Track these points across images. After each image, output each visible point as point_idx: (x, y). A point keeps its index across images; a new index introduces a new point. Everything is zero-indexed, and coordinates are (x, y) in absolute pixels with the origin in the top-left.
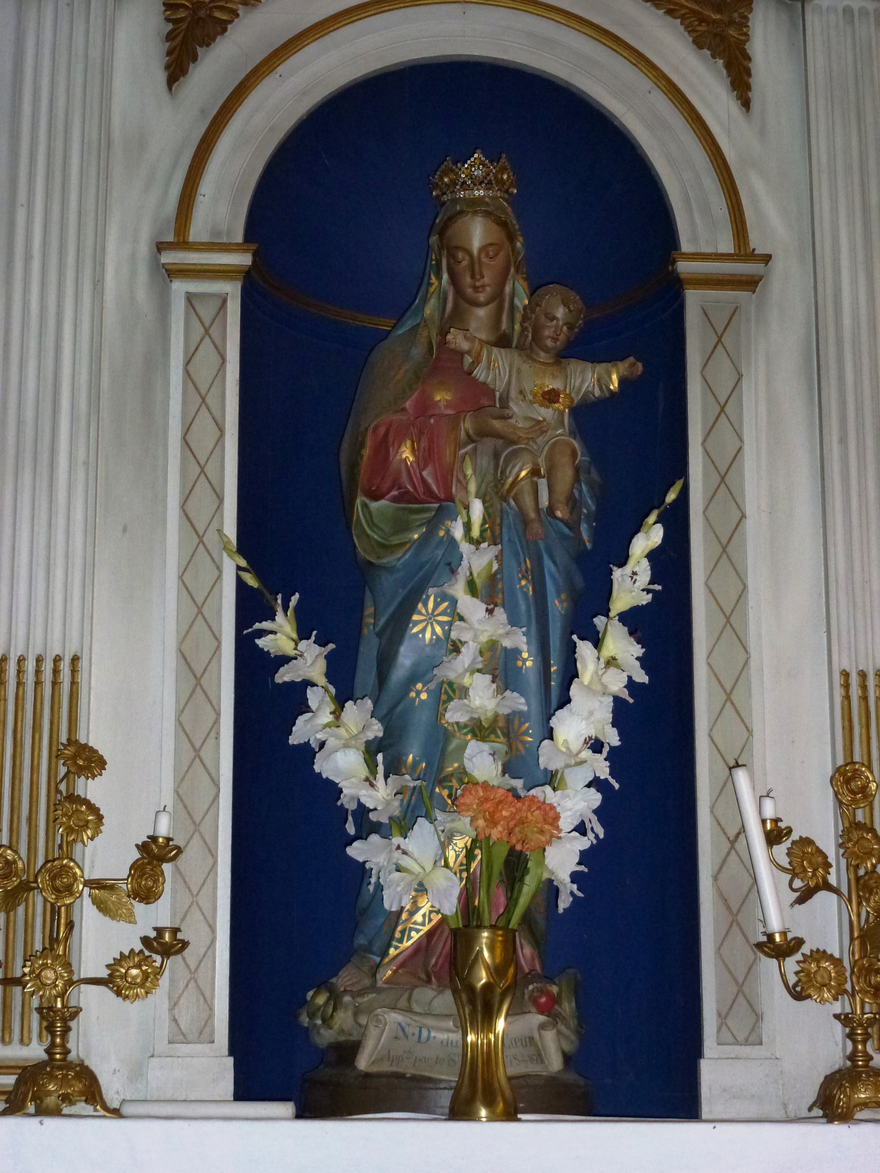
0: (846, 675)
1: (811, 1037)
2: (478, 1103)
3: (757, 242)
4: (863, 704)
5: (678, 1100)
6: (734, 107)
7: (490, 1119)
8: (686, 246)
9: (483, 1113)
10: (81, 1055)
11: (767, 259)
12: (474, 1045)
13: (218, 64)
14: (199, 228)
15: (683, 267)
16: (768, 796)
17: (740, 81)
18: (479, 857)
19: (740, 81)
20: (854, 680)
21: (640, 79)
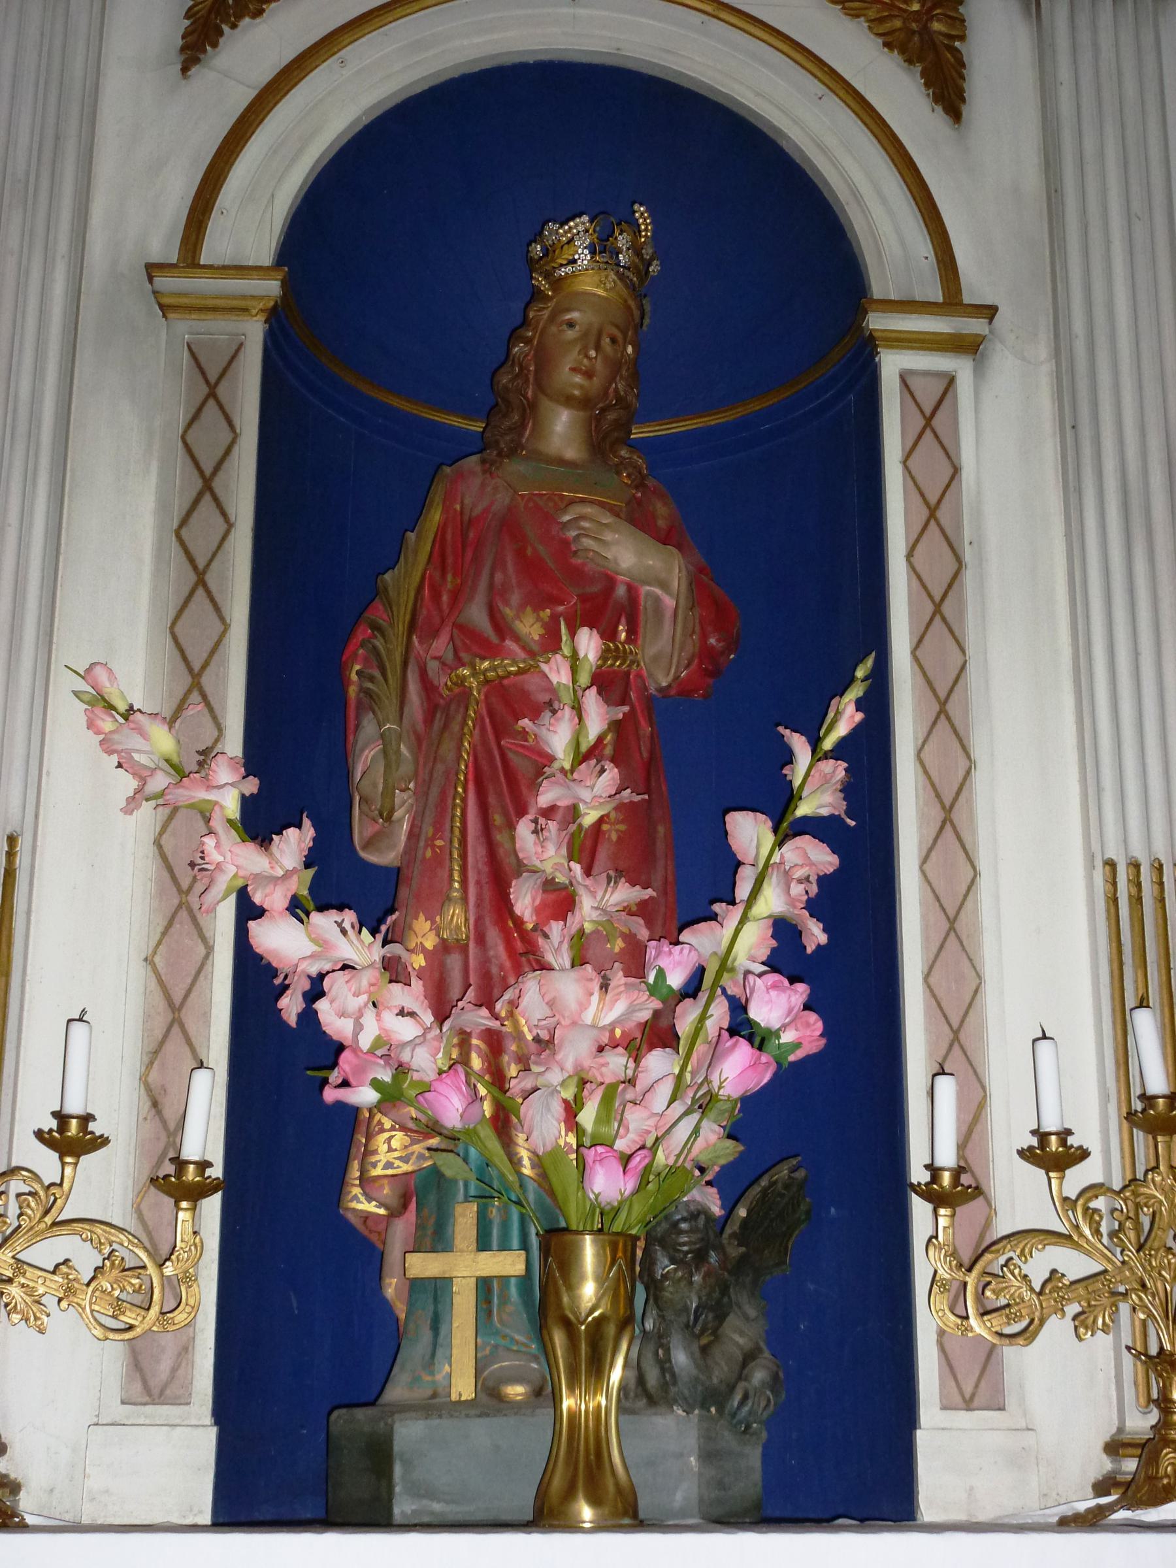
0: (1111, 864)
1: (1070, 1391)
2: (581, 1495)
3: (976, 282)
4: (1159, 905)
5: (879, 1492)
6: (937, 119)
7: (600, 1527)
8: (879, 287)
9: (586, 1513)
10: (646, 997)
11: (990, 312)
12: (573, 1416)
13: (252, 51)
14: (217, 246)
15: (876, 322)
16: (80, 1020)
17: (948, 90)
18: (648, 588)
19: (948, 90)
20: (1145, 870)
21: (810, 90)
